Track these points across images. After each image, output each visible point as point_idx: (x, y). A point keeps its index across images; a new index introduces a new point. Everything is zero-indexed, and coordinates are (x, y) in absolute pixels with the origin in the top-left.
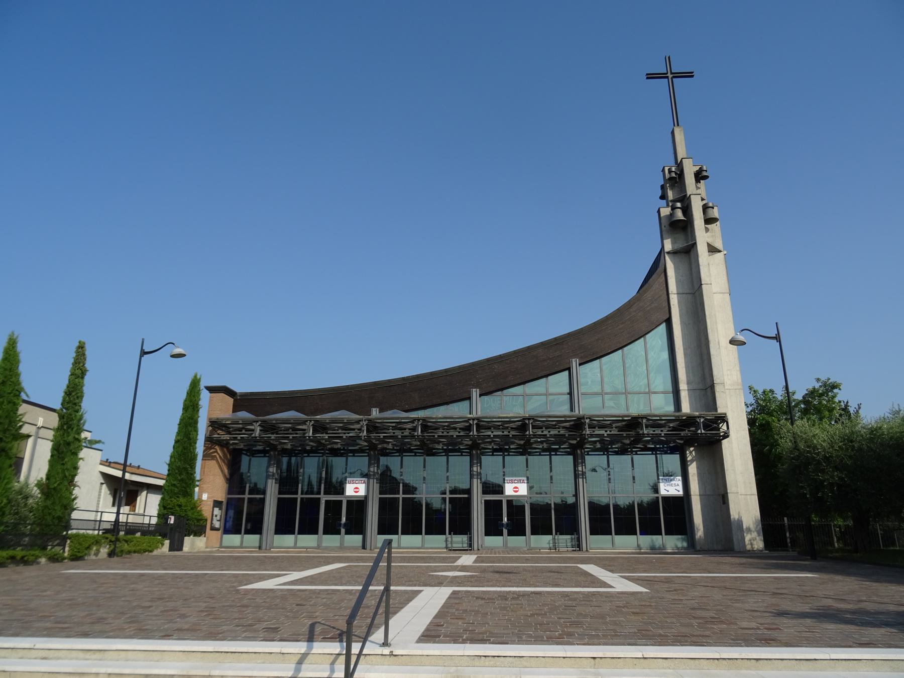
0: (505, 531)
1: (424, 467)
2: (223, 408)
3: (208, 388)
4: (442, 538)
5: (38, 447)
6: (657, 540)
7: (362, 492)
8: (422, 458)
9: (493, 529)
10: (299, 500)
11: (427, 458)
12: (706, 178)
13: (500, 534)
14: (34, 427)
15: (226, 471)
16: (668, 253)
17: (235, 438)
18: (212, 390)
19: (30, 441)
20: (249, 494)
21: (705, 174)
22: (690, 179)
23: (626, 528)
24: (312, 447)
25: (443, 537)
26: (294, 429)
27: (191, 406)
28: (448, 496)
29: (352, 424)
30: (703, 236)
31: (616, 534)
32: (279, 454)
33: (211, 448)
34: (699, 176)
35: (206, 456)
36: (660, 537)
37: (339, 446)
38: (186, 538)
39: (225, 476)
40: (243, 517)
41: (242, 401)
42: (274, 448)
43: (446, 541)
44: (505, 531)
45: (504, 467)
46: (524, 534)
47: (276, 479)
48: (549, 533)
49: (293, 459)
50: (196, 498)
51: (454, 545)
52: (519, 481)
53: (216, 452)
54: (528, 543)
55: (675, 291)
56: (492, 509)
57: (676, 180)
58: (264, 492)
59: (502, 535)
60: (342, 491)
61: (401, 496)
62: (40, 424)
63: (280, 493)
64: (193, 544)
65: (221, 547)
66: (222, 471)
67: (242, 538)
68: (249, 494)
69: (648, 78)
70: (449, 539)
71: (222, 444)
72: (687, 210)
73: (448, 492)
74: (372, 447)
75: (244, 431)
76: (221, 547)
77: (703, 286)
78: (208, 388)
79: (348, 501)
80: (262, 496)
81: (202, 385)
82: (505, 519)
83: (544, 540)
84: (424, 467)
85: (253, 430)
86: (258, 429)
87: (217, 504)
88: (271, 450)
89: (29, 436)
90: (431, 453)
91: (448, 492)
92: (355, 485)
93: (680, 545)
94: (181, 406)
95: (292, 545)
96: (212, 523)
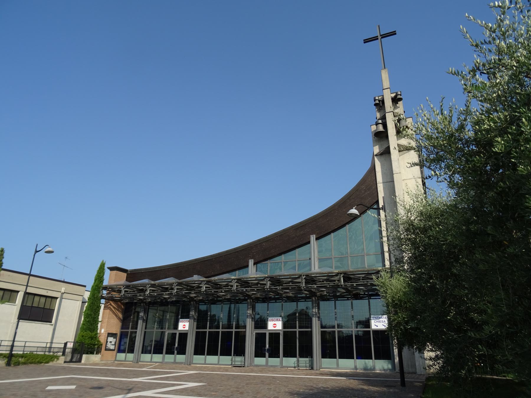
0: (267, 354)
1: (352, 308)
2: (121, 279)
3: (109, 268)
4: (229, 358)
5: (62, 303)
6: (369, 363)
7: (187, 328)
8: (349, 302)
9: (259, 353)
10: (166, 334)
11: (355, 302)
12: (400, 99)
13: (264, 356)
14: (60, 294)
15: (121, 316)
16: (376, 155)
17: (253, 290)
18: (112, 269)
19: (58, 300)
20: (236, 329)
21: (399, 97)
22: (388, 103)
23: (346, 354)
24: (306, 294)
25: (230, 357)
26: (293, 282)
27: (99, 278)
28: (336, 330)
29: (296, 278)
30: (393, 140)
31: (339, 358)
32: (318, 299)
33: (108, 303)
34: (395, 100)
35: (105, 307)
36: (371, 361)
37: (325, 293)
38: (84, 355)
39: (119, 318)
40: (126, 343)
41: (133, 275)
42: (249, 297)
43: (232, 360)
44: (267, 354)
45: (335, 308)
46: (279, 357)
47: (194, 319)
48: (295, 356)
49: (233, 306)
50: (99, 332)
51: (236, 363)
52: (277, 320)
53: (111, 305)
54: (281, 362)
55: (381, 181)
56: (260, 339)
57: (380, 105)
58: (245, 327)
59: (265, 357)
60: (265, 326)
61: (234, 330)
62: (63, 291)
63: (197, 328)
64: (87, 359)
65: (116, 360)
66: (116, 316)
67: (206, 357)
68: (236, 329)
69: (365, 43)
70: (234, 359)
71: (112, 299)
72: (385, 126)
73: (336, 326)
74: (312, 294)
75: (259, 285)
76: (116, 360)
77: (394, 175)
78: (109, 268)
79: (180, 333)
80: (310, 330)
81: (106, 266)
82: (267, 346)
83: (291, 361)
84: (352, 308)
85: (265, 284)
86: (269, 283)
87: (110, 335)
88: (248, 299)
89: (57, 298)
90: (357, 297)
91: (336, 326)
92: (274, 322)
93: (386, 367)
94: (94, 279)
95: (149, 360)
96: (106, 346)
